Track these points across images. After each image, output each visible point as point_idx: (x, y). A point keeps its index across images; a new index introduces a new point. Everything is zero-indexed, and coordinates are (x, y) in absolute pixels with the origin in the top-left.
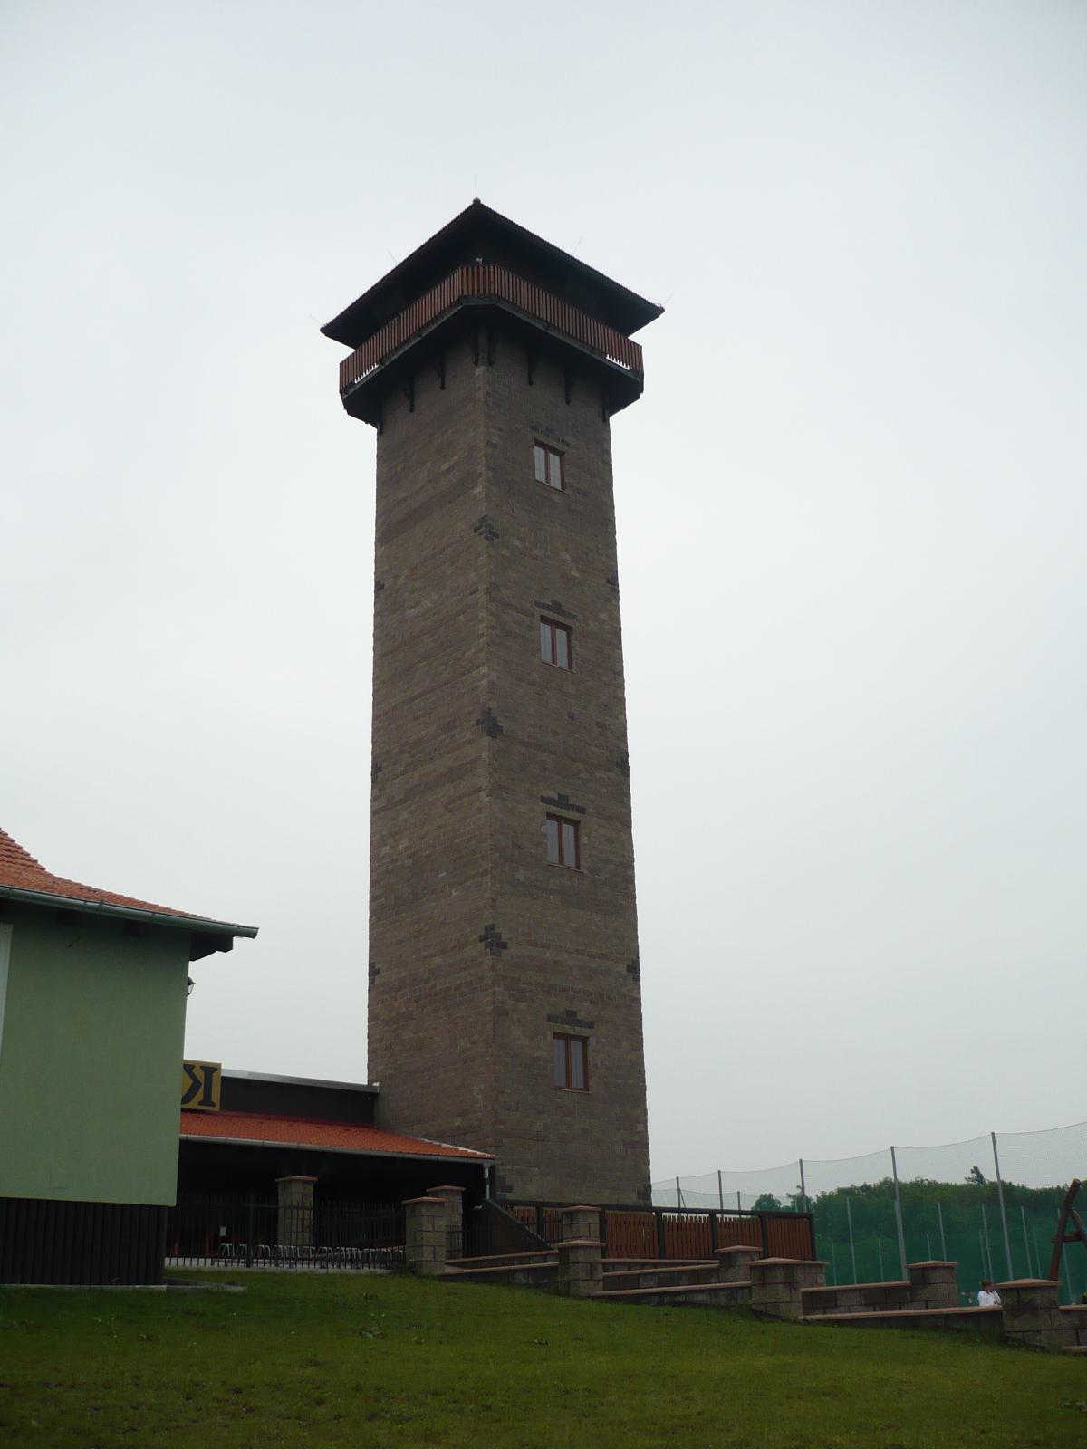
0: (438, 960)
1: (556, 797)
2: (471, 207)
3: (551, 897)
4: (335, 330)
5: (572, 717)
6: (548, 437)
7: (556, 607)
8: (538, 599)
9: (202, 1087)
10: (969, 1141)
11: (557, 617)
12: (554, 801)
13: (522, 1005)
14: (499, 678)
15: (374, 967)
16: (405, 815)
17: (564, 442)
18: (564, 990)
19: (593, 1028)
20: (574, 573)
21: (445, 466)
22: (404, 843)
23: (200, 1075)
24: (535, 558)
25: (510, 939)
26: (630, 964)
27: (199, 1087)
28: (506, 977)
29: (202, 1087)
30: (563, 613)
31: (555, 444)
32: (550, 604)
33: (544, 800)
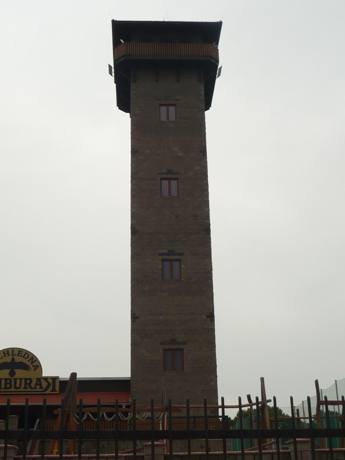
2: (215, 22)
3: (163, 294)
5: (177, 216)
7: (170, 172)
9: (51, 386)
10: (339, 380)
11: (169, 176)
23: (51, 381)
26: (209, 314)
27: (51, 385)
29: (51, 386)
30: (174, 173)
31: (171, 102)
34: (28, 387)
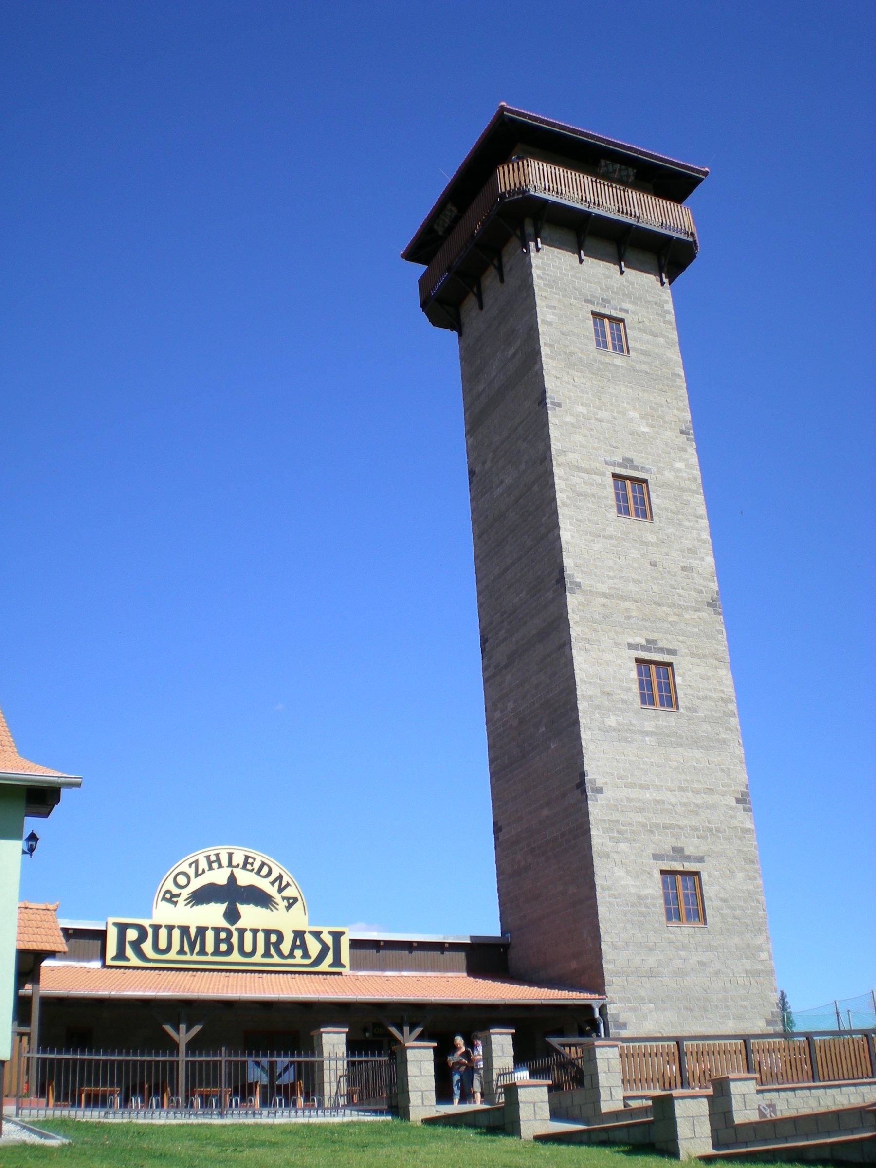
0: (546, 812)
1: (644, 643)
4: (414, 253)
5: (654, 564)
6: (605, 307)
8: (608, 459)
12: (642, 646)
13: (623, 846)
14: (572, 537)
15: (497, 825)
16: (509, 677)
17: (622, 310)
18: (670, 827)
19: (704, 862)
20: (645, 429)
21: (511, 352)
22: (511, 705)
23: (329, 940)
24: (601, 421)
25: (606, 783)
28: (605, 821)
30: (637, 468)
32: (621, 461)
33: (631, 646)
34: (272, 951)
